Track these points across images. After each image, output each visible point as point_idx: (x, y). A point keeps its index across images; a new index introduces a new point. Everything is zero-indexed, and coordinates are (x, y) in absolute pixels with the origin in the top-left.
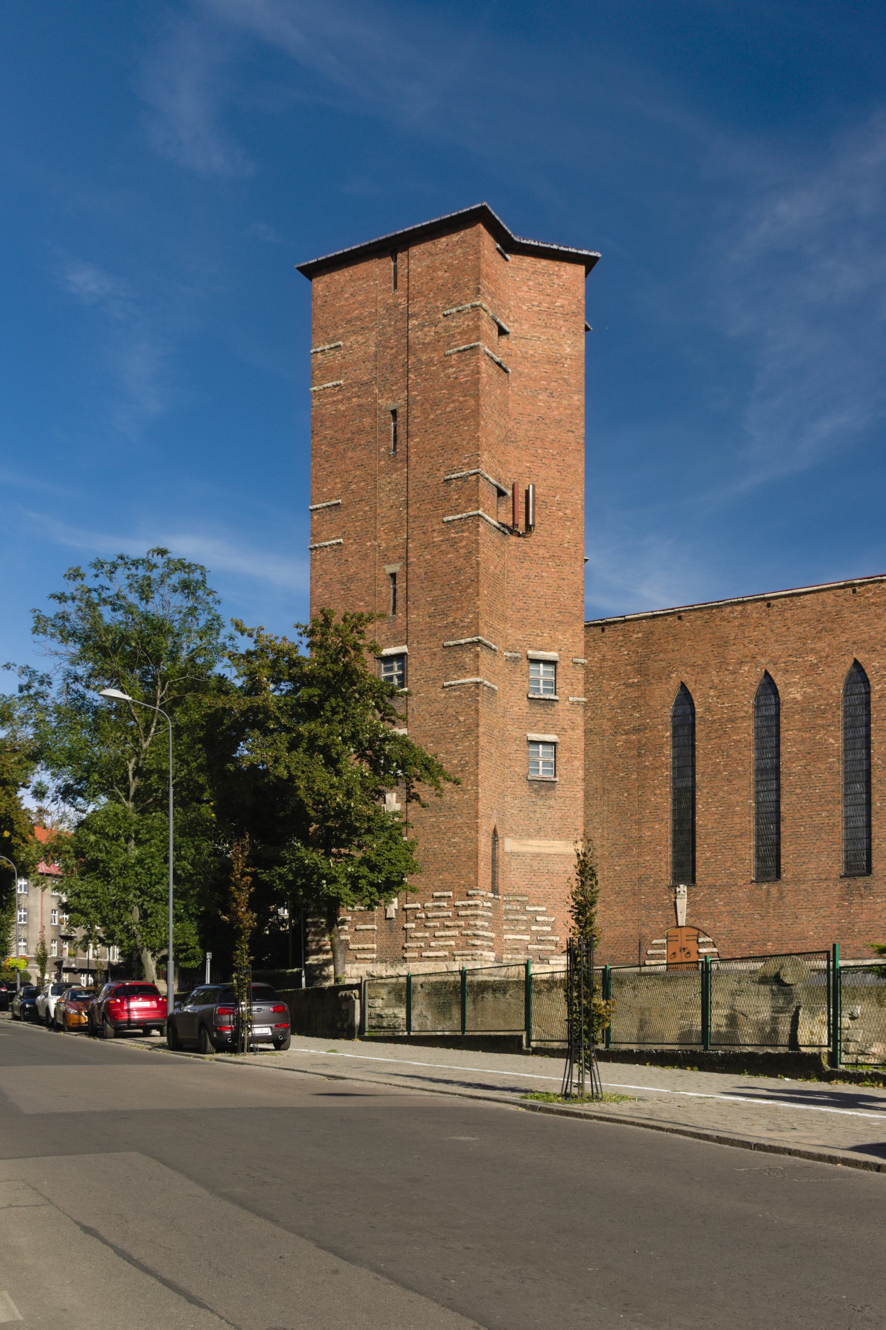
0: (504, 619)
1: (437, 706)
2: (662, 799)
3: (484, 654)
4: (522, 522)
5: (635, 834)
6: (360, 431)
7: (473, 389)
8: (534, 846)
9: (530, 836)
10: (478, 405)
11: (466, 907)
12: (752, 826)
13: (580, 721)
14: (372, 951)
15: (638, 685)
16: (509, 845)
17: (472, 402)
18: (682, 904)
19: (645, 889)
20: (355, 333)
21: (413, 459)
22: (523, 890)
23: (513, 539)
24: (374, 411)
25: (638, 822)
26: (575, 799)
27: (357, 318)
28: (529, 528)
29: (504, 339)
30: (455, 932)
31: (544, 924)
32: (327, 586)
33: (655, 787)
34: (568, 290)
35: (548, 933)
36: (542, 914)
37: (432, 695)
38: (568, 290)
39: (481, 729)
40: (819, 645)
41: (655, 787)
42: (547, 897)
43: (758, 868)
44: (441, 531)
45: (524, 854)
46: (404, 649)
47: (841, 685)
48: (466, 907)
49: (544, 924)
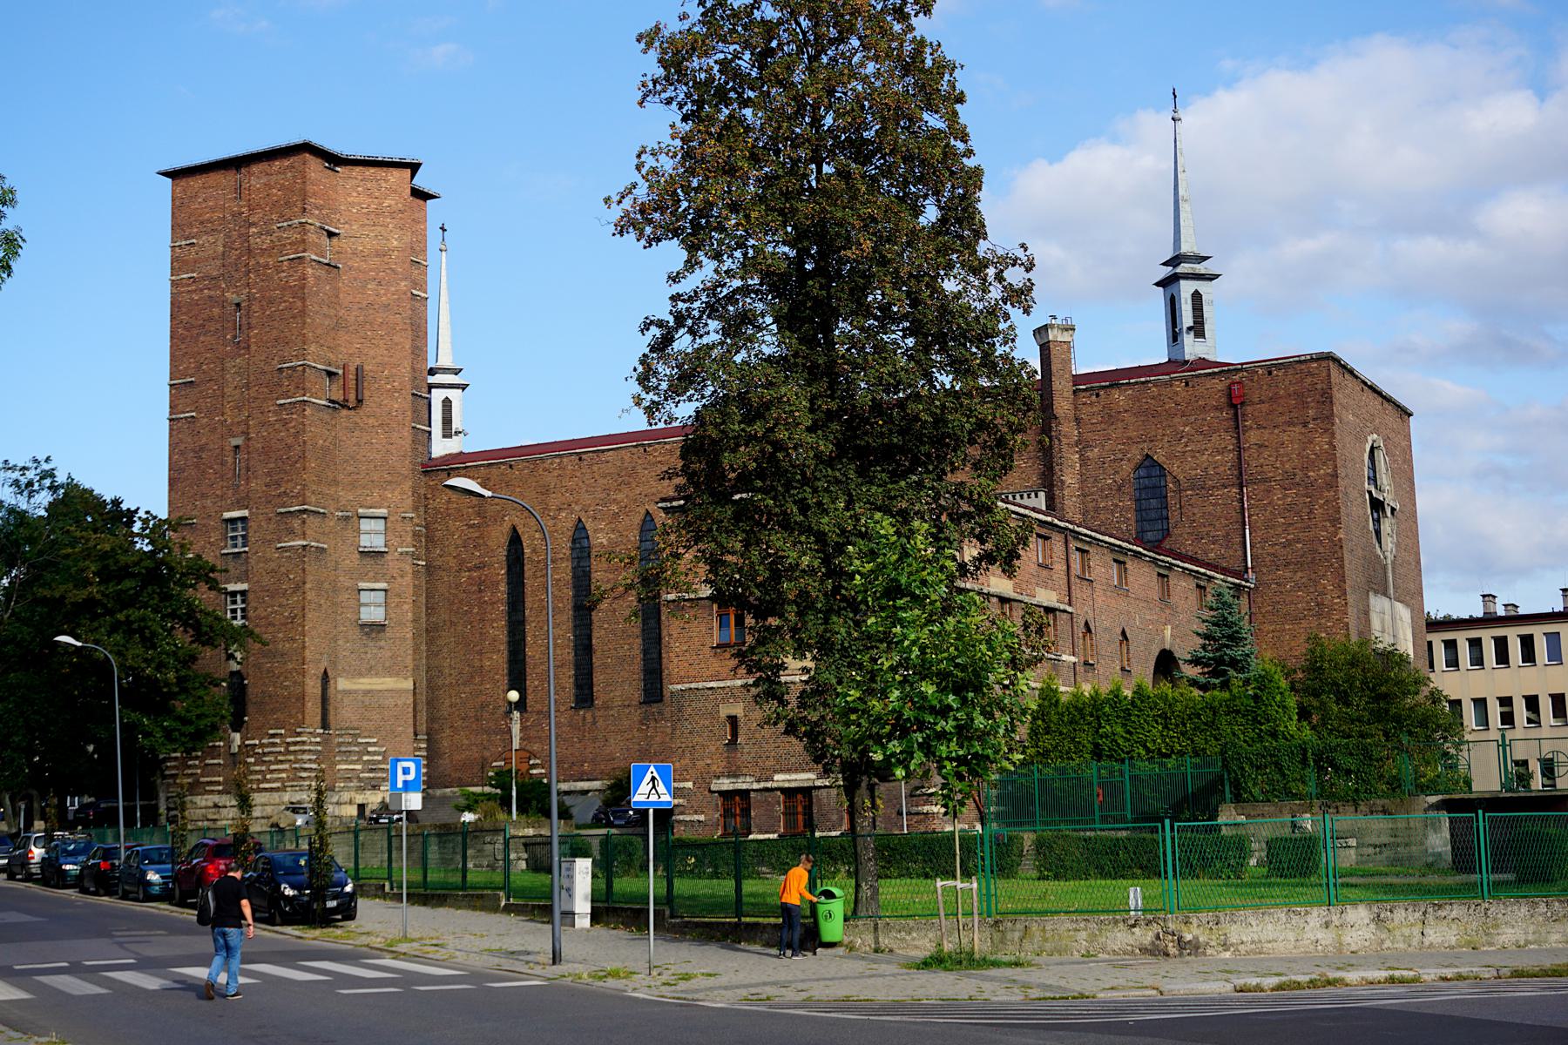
0: (335, 482)
1: (273, 565)
2: (498, 630)
3: (311, 520)
4: (352, 397)
5: (477, 664)
6: (211, 319)
7: (300, 291)
8: (365, 683)
9: (361, 675)
10: (304, 306)
11: (295, 743)
12: (571, 657)
13: (408, 568)
14: (218, 783)
15: (479, 526)
16: (342, 684)
17: (299, 304)
18: (516, 729)
19: (486, 715)
20: (206, 233)
21: (253, 348)
22: (355, 724)
23: (344, 412)
24: (223, 303)
25: (480, 653)
26: (405, 639)
27: (209, 221)
28: (360, 401)
29: (335, 240)
30: (286, 766)
31: (375, 753)
32: (182, 453)
33: (493, 621)
34: (395, 191)
35: (379, 762)
36: (374, 744)
37: (268, 555)
38: (395, 191)
39: (308, 586)
40: (620, 496)
41: (493, 621)
42: (377, 730)
43: (577, 696)
44: (275, 412)
45: (356, 691)
46: (245, 513)
47: (637, 532)
48: (295, 743)
49: (375, 753)
